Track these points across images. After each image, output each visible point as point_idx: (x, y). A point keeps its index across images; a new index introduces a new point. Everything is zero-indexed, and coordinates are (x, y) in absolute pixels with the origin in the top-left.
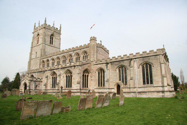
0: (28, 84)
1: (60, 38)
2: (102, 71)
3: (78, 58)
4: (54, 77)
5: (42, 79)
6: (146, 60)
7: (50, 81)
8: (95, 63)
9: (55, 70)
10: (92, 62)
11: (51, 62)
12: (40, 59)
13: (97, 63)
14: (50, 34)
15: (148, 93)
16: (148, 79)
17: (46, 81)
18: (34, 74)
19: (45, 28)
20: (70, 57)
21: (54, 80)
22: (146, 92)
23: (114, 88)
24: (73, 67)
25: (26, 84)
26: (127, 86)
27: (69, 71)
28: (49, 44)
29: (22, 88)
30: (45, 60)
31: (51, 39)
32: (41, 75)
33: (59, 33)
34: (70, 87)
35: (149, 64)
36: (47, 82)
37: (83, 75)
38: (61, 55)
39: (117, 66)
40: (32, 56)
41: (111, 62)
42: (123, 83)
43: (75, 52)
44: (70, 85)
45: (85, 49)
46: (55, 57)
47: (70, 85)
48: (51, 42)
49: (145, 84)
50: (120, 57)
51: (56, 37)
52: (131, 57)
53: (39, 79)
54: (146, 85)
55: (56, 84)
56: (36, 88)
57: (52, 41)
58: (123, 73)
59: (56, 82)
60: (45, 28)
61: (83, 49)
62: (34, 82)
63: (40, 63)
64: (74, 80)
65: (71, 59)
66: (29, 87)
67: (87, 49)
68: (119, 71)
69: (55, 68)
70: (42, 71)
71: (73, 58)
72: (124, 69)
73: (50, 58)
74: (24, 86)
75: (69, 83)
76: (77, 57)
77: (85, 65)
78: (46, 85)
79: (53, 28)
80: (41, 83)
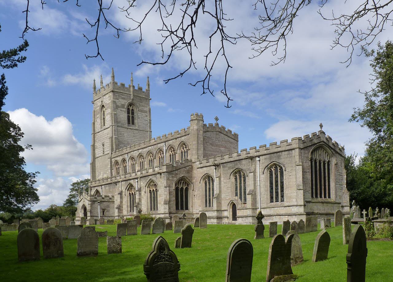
0: (88, 208)
1: (150, 109)
2: (208, 178)
3: (173, 155)
4: (132, 193)
5: (113, 197)
6: (275, 159)
7: (126, 200)
8: (200, 166)
9: (132, 180)
10: (194, 163)
11: (129, 164)
12: (111, 159)
13: (202, 165)
14: (126, 102)
15: (274, 217)
16: (277, 193)
17: (119, 200)
18: (99, 189)
19: (113, 91)
20: (161, 154)
21: (208, 187)
22: (272, 216)
23: (227, 210)
24: (158, 176)
25: (85, 207)
26: (246, 205)
27: (152, 181)
28: (126, 126)
29: (80, 214)
30: (119, 159)
31: (128, 113)
32: (111, 190)
33: (147, 98)
34: (184, 208)
35: (279, 166)
36: (121, 202)
37: (177, 189)
38: (145, 150)
39: (232, 170)
40: (97, 151)
41: (222, 163)
42: (241, 200)
43: (167, 143)
44: (327, 194)
45: (183, 138)
46: (135, 154)
47: (327, 194)
48: (131, 120)
49: (273, 202)
50: (245, 152)
51: (140, 108)
52: (253, 153)
53: (108, 198)
54: (274, 203)
55: (213, 196)
56: (103, 214)
57: (133, 117)
58: (240, 183)
59: (213, 193)
60: (113, 91)
61: (180, 137)
62: (99, 203)
63: (111, 166)
64: (161, 198)
65: (162, 158)
66: (91, 212)
67: (185, 137)
68: (236, 179)
69: (131, 178)
70: (136, 177)
71: (165, 155)
72: (279, 171)
73: (127, 155)
74: (83, 212)
75: (154, 204)
76: (171, 154)
77: (179, 170)
78: (120, 208)
79: (132, 89)
80: (111, 205)
